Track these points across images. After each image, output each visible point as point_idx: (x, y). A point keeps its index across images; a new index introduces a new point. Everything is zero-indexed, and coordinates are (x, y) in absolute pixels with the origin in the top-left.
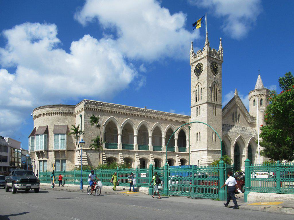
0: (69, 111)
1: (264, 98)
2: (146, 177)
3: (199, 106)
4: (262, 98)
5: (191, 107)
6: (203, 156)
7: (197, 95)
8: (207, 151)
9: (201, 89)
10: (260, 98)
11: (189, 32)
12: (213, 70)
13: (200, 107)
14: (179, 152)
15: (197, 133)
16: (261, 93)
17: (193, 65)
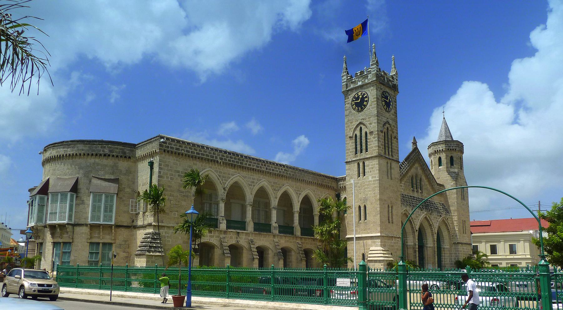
0: (125, 153)
1: (443, 156)
2: (338, 280)
4: (453, 155)
7: (358, 143)
9: (366, 133)
10: (437, 156)
11: (533, 57)
12: (386, 104)
13: (364, 163)
16: (450, 147)
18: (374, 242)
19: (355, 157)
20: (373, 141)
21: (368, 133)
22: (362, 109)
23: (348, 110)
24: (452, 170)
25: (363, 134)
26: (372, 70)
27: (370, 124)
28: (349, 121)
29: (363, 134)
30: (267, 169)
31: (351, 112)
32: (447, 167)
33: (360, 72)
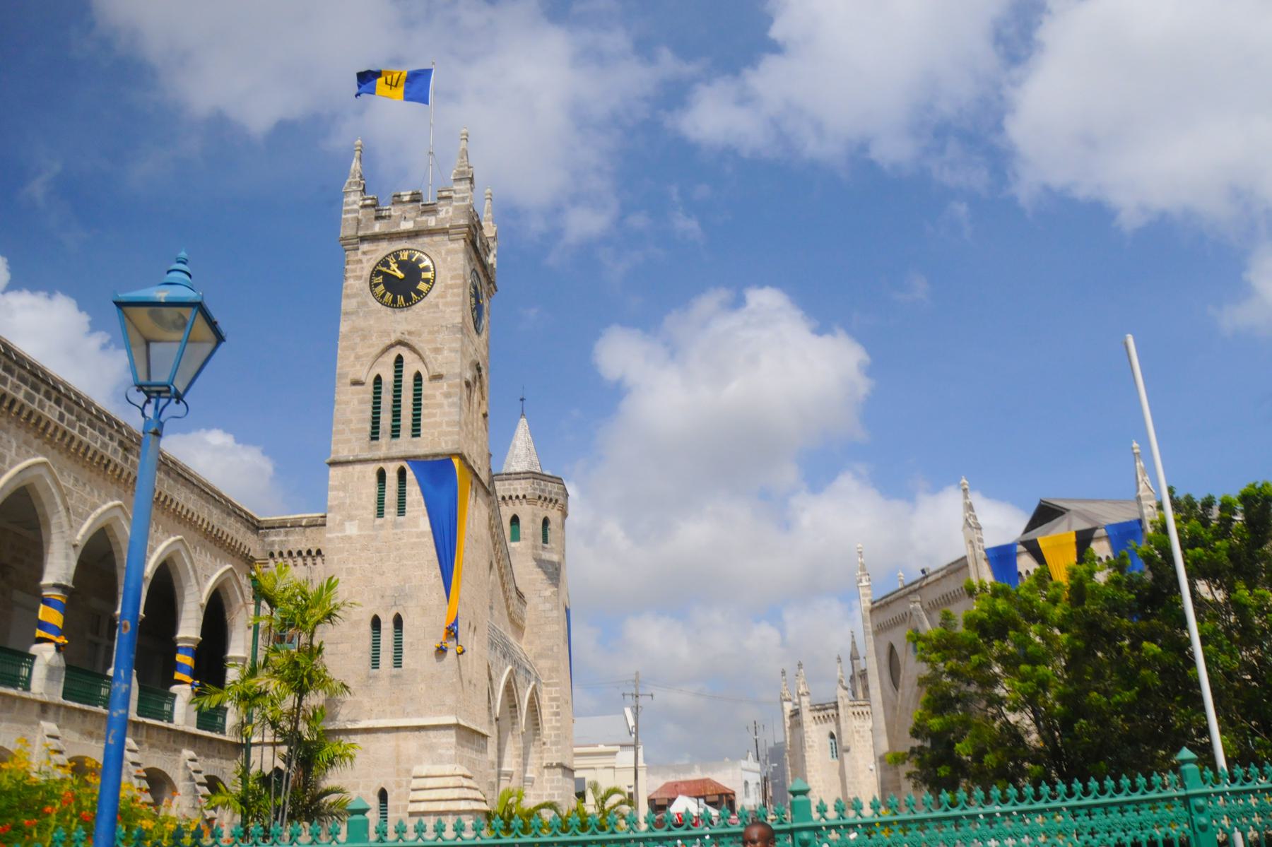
3: (382, 465)
5: (333, 464)
6: (419, 761)
8: (453, 732)
9: (418, 377)
14: (141, 719)
15: (376, 623)
16: (543, 491)
17: (365, 247)
18: (431, 748)
19: (370, 448)
20: (441, 406)
21: (425, 377)
22: (409, 302)
23: (354, 296)
24: (546, 556)
25: (408, 380)
26: (458, 196)
27: (437, 350)
28: (354, 330)
29: (408, 380)
30: (61, 417)
31: (365, 304)
32: (535, 547)
33: (410, 192)
